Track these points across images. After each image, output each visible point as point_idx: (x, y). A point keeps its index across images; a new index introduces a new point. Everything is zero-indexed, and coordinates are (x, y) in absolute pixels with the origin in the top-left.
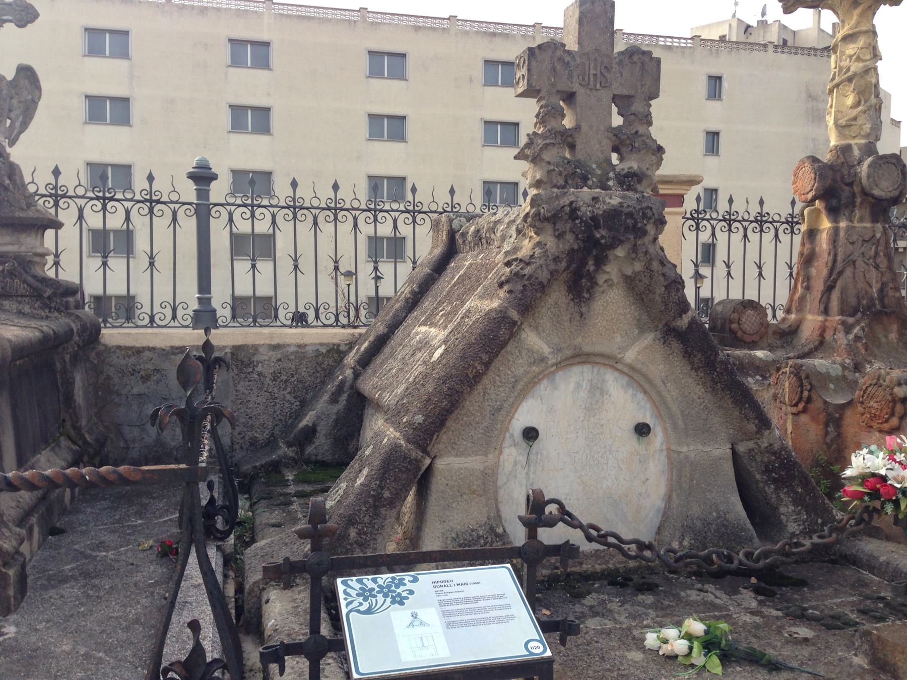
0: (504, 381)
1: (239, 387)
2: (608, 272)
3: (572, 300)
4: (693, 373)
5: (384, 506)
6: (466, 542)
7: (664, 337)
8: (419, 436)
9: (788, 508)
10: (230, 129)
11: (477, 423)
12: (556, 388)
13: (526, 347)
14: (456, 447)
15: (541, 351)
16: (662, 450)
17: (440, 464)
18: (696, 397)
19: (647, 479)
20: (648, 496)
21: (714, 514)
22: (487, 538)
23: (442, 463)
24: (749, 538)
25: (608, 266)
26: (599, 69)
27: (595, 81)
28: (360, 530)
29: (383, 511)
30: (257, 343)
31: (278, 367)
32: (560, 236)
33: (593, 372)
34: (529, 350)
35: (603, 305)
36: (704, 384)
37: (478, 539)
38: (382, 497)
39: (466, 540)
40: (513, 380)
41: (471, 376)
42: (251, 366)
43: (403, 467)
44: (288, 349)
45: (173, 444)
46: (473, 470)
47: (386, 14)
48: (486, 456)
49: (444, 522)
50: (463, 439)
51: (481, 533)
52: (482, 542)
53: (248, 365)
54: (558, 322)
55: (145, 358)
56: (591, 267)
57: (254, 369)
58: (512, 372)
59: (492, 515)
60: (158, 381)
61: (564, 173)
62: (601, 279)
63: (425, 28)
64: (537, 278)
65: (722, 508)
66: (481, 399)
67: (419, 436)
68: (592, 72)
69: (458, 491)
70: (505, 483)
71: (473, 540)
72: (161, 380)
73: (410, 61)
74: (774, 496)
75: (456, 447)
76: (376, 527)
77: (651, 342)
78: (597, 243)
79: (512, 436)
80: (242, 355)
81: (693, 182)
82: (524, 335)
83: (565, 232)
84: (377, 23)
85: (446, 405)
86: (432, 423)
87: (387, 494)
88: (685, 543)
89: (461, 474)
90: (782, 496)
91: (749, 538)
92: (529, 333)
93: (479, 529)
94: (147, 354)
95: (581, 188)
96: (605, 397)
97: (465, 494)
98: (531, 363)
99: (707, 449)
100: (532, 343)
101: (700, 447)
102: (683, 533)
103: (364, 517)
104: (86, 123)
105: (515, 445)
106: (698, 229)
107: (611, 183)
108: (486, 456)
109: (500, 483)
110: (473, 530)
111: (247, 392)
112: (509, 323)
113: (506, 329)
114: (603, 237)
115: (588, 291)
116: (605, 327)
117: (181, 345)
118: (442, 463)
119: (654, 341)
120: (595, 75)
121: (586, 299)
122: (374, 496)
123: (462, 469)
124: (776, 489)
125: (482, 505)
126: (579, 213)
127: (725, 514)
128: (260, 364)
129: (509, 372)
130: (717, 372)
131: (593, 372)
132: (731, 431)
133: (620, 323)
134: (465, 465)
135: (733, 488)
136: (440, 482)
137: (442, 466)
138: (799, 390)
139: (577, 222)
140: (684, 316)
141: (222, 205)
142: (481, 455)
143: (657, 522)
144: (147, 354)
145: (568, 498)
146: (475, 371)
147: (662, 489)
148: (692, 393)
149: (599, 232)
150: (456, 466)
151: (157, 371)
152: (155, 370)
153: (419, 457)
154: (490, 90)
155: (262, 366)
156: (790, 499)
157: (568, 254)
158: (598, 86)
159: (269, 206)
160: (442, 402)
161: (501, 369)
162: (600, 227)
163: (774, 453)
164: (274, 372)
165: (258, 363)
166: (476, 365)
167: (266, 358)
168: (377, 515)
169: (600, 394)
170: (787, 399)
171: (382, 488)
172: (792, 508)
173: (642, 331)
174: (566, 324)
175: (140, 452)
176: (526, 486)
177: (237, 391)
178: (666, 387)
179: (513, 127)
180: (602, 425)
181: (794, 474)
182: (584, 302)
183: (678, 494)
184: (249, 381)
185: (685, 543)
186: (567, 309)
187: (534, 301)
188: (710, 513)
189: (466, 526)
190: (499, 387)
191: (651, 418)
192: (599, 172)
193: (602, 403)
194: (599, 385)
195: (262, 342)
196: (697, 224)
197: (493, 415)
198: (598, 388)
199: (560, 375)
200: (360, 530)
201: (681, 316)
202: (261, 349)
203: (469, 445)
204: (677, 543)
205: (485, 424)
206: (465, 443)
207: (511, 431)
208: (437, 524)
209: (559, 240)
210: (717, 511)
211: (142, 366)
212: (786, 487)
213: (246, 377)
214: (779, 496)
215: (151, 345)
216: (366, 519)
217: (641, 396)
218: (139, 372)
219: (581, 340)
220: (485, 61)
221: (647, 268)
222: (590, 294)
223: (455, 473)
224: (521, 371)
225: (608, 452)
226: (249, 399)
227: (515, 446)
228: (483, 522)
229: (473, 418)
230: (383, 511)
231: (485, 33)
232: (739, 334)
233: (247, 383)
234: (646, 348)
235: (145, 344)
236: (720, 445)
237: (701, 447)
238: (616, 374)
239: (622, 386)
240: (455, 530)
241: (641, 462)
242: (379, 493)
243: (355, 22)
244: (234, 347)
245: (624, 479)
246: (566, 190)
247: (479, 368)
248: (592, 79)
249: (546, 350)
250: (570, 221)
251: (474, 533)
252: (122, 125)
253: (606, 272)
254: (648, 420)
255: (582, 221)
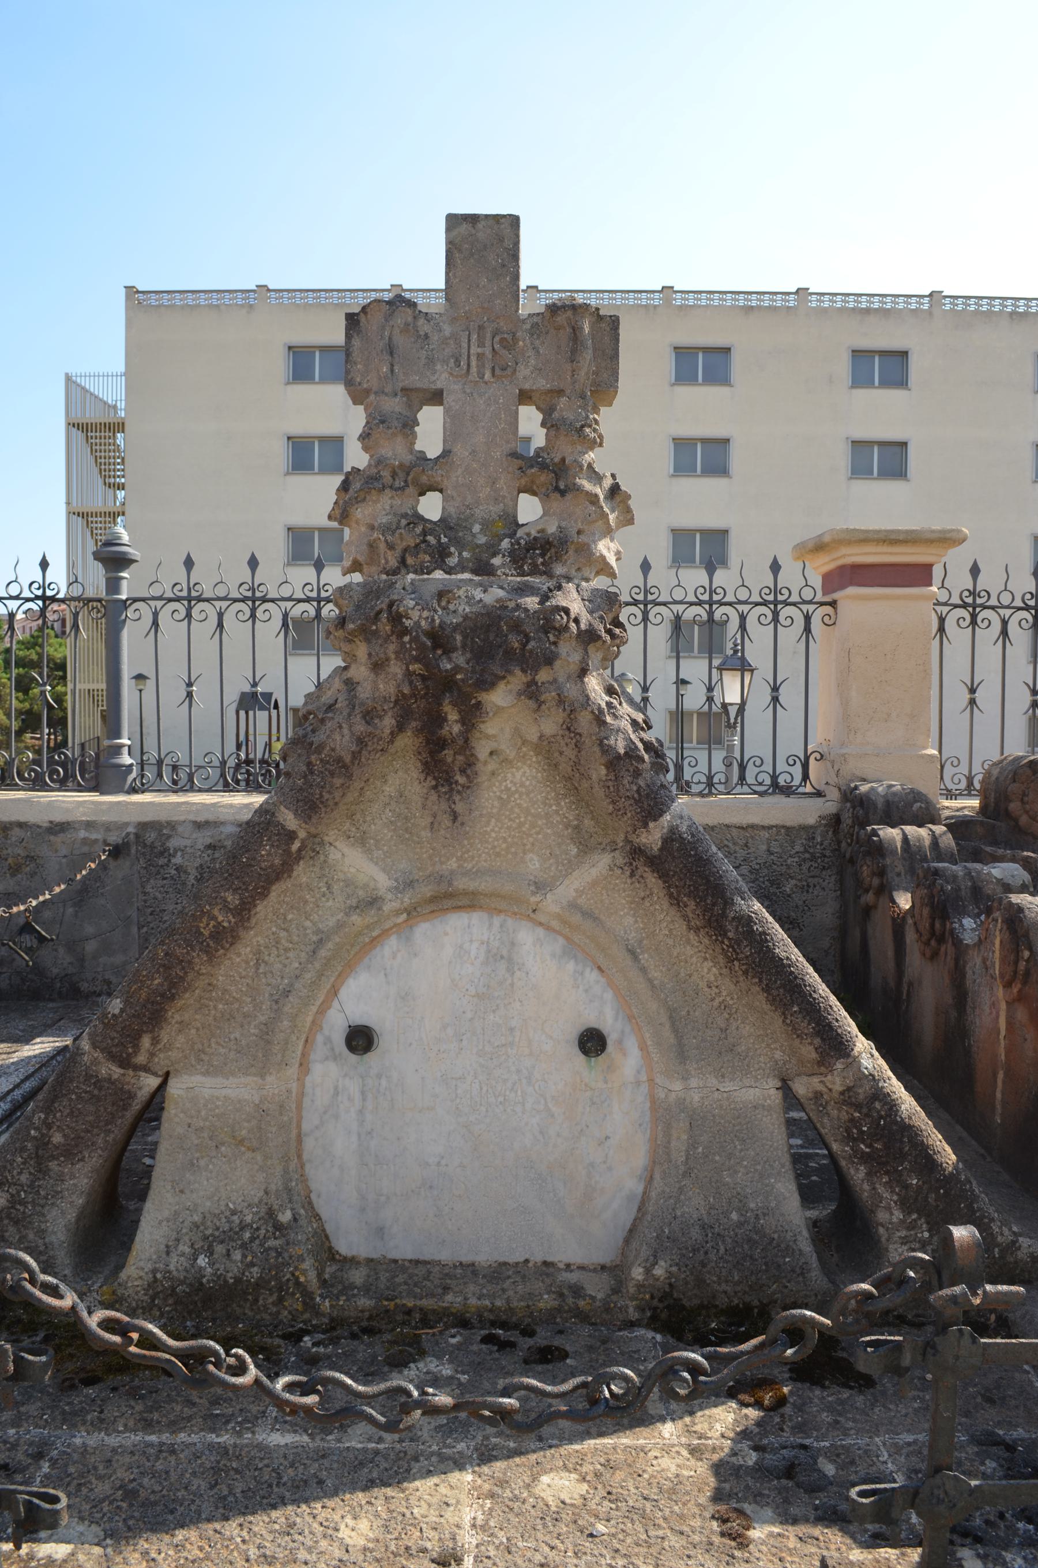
0: (295, 938)
1: (149, 889)
2: (494, 736)
3: (435, 787)
4: (692, 935)
5: (53, 1158)
6: (217, 1233)
7: (631, 864)
8: (112, 1039)
9: (892, 1214)
10: (672, 471)
11: (246, 1016)
12: (415, 955)
13: (341, 876)
14: (206, 1058)
15: (372, 884)
16: (638, 1083)
17: (176, 1088)
18: (703, 985)
19: (607, 1138)
20: (610, 1169)
21: (734, 1216)
22: (258, 1229)
23: (178, 1086)
24: (798, 1271)
25: (488, 724)
26: (488, 343)
27: (481, 367)
28: (12, 1196)
29: (53, 1165)
30: (174, 819)
31: (206, 858)
32: (378, 666)
33: (491, 925)
34: (348, 883)
35: (500, 798)
36: (713, 959)
37: (242, 1229)
38: (49, 1142)
39: (218, 1229)
40: (315, 938)
41: (206, 933)
42: (166, 854)
43: (86, 1092)
44: (222, 829)
45: (55, 971)
46: (239, 1101)
47: (701, 292)
48: (263, 1077)
49: (182, 1192)
50: (218, 1043)
51: (248, 1219)
52: (247, 1235)
53: (162, 854)
54: (406, 830)
55: (14, 839)
56: (453, 726)
57: (169, 861)
58: (314, 924)
59: (273, 1187)
60: (33, 874)
61: (400, 547)
62: (482, 750)
63: (759, 307)
64: (333, 750)
65: (752, 1205)
66: (251, 972)
67: (112, 1039)
68: (474, 350)
69: (211, 1138)
70: (317, 1128)
71: (231, 1229)
72: (36, 873)
73: (737, 359)
74: (866, 1187)
75: (206, 1058)
76: (42, 1193)
77: (604, 872)
78: (447, 684)
79: (328, 1040)
80: (151, 836)
81: (948, 540)
82: (334, 855)
83: (388, 659)
84: (688, 306)
85: (161, 985)
86: (134, 1016)
87: (57, 1138)
88: (659, 1271)
89: (217, 1107)
90: (881, 1189)
91: (798, 1271)
92: (346, 850)
93: (246, 1211)
94: (17, 832)
95: (428, 573)
96: (518, 974)
97: (223, 1144)
98: (351, 907)
99: (728, 1086)
100: (352, 870)
101: (713, 1082)
102: (655, 1251)
103: (20, 1173)
104: (288, 474)
105: (335, 1057)
106: (974, 622)
107: (497, 561)
108: (263, 1077)
109: (306, 1127)
110: (234, 1213)
111: (159, 896)
112: (278, 834)
113: (272, 846)
114: (457, 669)
115: (463, 771)
116: (505, 839)
117: (64, 820)
118: (178, 1086)
119: (611, 869)
120: (480, 356)
121: (463, 787)
122: (35, 1138)
123: (218, 1098)
124: (869, 1174)
125: (256, 1167)
126: (408, 623)
127: (757, 1217)
128: (179, 854)
129: (308, 924)
130: (730, 939)
131: (491, 925)
132: (778, 1054)
133: (538, 833)
134: (224, 1092)
135: (783, 1166)
136: (177, 1120)
137: (181, 1092)
138: (1012, 957)
139: (407, 639)
140: (651, 825)
141: (143, 600)
142: (255, 1075)
143: (627, 1219)
144: (17, 832)
145: (443, 1162)
146: (212, 923)
147: (640, 1158)
148: (695, 977)
149: (450, 660)
150: (207, 1093)
151: (31, 858)
152: (28, 856)
153: (115, 1076)
154: (861, 394)
155: (183, 856)
156: (895, 1198)
157: (396, 702)
158: (488, 375)
159: (278, 600)
160: (153, 979)
161: (290, 917)
162: (454, 649)
163: (858, 1107)
164: (201, 865)
165: (176, 851)
166: (216, 912)
167: (188, 842)
168: (42, 1171)
169: (508, 970)
170: (997, 972)
171: (49, 1127)
172: (898, 1215)
173: (586, 847)
174: (423, 833)
175: (10, 979)
176: (359, 1135)
177: (145, 893)
178: (639, 961)
179: (897, 449)
180: (512, 1030)
181: (901, 1150)
182: (459, 792)
183: (664, 1172)
184: (165, 879)
185: (659, 1271)
186: (424, 807)
187: (329, 792)
188: (726, 1214)
189: (222, 1203)
190: (286, 950)
191: (616, 1019)
192: (482, 540)
193: (512, 985)
194: (505, 953)
195: (182, 818)
196: (974, 617)
197: (277, 1002)
198: (502, 957)
199: (423, 930)
200: (12, 1196)
201: (645, 825)
202: (180, 829)
203: (232, 1055)
204: (641, 1270)
205: (262, 1019)
206: (222, 1051)
207: (326, 1032)
208: (168, 1195)
209: (377, 674)
210: (742, 1210)
211: (10, 851)
212: (887, 1173)
213: (158, 873)
214: (874, 1189)
215: (22, 819)
216: (24, 1178)
217: (592, 975)
218: (6, 860)
219: (455, 866)
220: (853, 351)
221: (569, 729)
222: (468, 777)
223: (205, 1105)
224: (332, 922)
225: (524, 1081)
226: (163, 907)
227: (335, 1059)
228: (256, 1200)
229: (236, 1006)
230: (53, 1165)
231: (853, 309)
232: (1024, 820)
233: (161, 882)
234: (594, 883)
235: (13, 819)
236: (757, 1080)
237: (714, 1081)
238: (540, 932)
239: (553, 955)
240: (201, 1210)
241: (593, 1103)
242: (43, 1135)
243: (655, 307)
244: (139, 824)
245: (558, 1135)
246: (394, 578)
247: (220, 918)
248: (474, 363)
249: (383, 882)
250: (394, 638)
251: (235, 1218)
252: (332, 474)
253: (488, 737)
254: (609, 1023)
255: (415, 639)
